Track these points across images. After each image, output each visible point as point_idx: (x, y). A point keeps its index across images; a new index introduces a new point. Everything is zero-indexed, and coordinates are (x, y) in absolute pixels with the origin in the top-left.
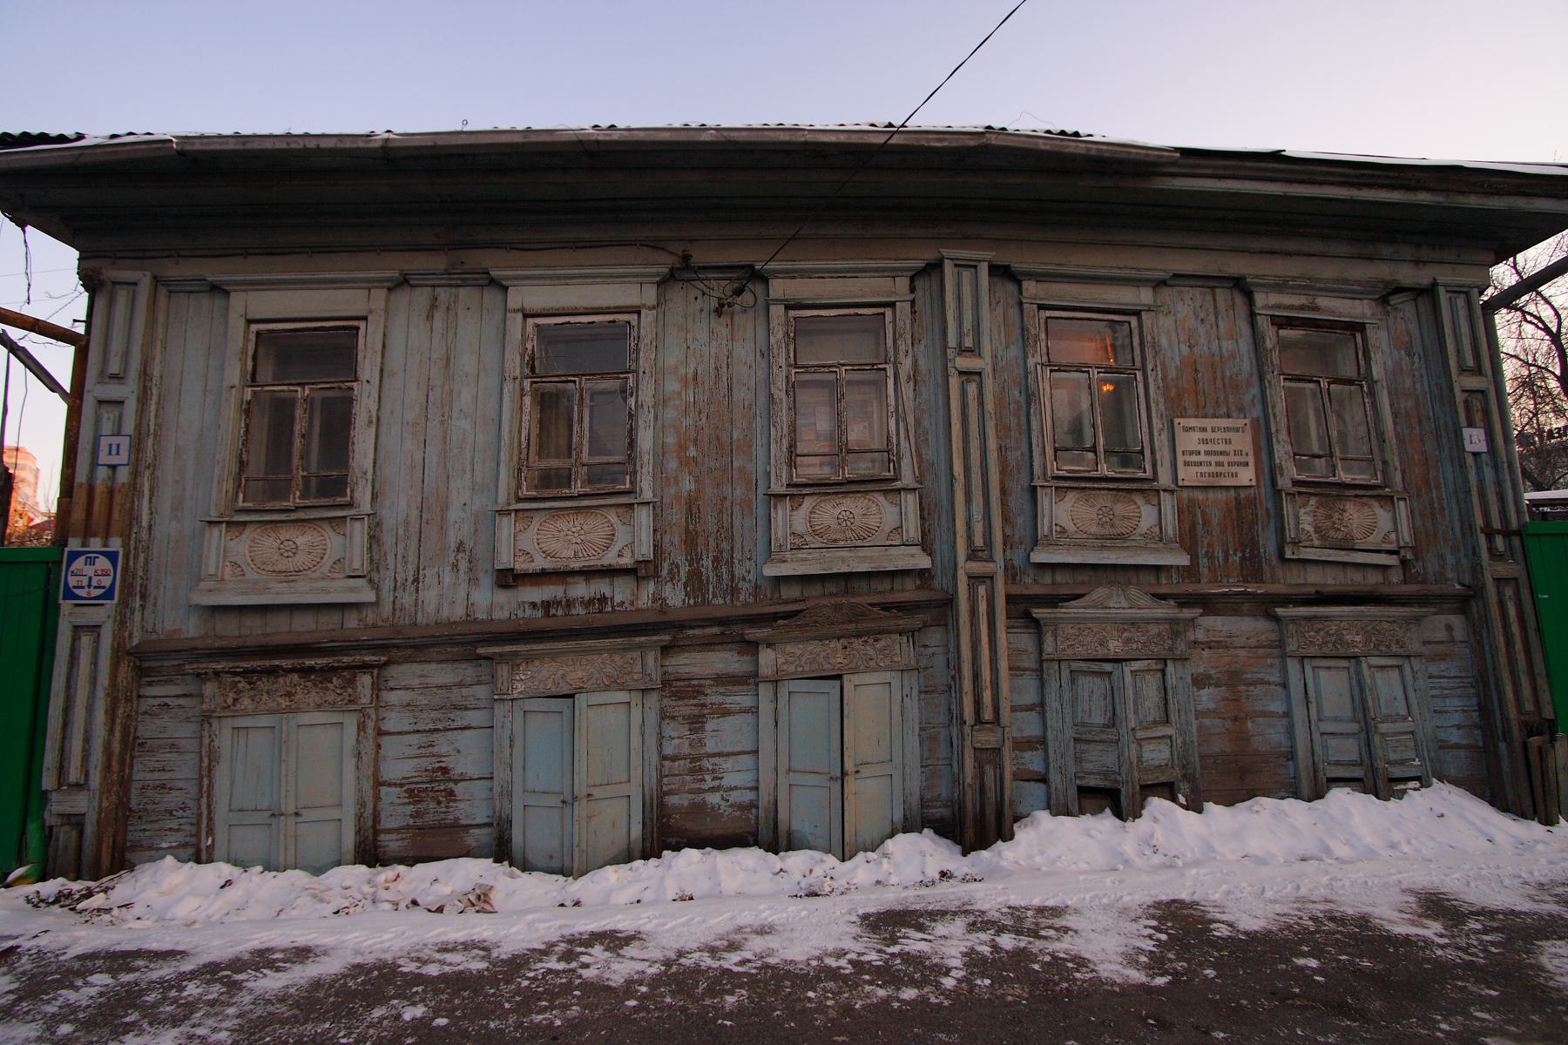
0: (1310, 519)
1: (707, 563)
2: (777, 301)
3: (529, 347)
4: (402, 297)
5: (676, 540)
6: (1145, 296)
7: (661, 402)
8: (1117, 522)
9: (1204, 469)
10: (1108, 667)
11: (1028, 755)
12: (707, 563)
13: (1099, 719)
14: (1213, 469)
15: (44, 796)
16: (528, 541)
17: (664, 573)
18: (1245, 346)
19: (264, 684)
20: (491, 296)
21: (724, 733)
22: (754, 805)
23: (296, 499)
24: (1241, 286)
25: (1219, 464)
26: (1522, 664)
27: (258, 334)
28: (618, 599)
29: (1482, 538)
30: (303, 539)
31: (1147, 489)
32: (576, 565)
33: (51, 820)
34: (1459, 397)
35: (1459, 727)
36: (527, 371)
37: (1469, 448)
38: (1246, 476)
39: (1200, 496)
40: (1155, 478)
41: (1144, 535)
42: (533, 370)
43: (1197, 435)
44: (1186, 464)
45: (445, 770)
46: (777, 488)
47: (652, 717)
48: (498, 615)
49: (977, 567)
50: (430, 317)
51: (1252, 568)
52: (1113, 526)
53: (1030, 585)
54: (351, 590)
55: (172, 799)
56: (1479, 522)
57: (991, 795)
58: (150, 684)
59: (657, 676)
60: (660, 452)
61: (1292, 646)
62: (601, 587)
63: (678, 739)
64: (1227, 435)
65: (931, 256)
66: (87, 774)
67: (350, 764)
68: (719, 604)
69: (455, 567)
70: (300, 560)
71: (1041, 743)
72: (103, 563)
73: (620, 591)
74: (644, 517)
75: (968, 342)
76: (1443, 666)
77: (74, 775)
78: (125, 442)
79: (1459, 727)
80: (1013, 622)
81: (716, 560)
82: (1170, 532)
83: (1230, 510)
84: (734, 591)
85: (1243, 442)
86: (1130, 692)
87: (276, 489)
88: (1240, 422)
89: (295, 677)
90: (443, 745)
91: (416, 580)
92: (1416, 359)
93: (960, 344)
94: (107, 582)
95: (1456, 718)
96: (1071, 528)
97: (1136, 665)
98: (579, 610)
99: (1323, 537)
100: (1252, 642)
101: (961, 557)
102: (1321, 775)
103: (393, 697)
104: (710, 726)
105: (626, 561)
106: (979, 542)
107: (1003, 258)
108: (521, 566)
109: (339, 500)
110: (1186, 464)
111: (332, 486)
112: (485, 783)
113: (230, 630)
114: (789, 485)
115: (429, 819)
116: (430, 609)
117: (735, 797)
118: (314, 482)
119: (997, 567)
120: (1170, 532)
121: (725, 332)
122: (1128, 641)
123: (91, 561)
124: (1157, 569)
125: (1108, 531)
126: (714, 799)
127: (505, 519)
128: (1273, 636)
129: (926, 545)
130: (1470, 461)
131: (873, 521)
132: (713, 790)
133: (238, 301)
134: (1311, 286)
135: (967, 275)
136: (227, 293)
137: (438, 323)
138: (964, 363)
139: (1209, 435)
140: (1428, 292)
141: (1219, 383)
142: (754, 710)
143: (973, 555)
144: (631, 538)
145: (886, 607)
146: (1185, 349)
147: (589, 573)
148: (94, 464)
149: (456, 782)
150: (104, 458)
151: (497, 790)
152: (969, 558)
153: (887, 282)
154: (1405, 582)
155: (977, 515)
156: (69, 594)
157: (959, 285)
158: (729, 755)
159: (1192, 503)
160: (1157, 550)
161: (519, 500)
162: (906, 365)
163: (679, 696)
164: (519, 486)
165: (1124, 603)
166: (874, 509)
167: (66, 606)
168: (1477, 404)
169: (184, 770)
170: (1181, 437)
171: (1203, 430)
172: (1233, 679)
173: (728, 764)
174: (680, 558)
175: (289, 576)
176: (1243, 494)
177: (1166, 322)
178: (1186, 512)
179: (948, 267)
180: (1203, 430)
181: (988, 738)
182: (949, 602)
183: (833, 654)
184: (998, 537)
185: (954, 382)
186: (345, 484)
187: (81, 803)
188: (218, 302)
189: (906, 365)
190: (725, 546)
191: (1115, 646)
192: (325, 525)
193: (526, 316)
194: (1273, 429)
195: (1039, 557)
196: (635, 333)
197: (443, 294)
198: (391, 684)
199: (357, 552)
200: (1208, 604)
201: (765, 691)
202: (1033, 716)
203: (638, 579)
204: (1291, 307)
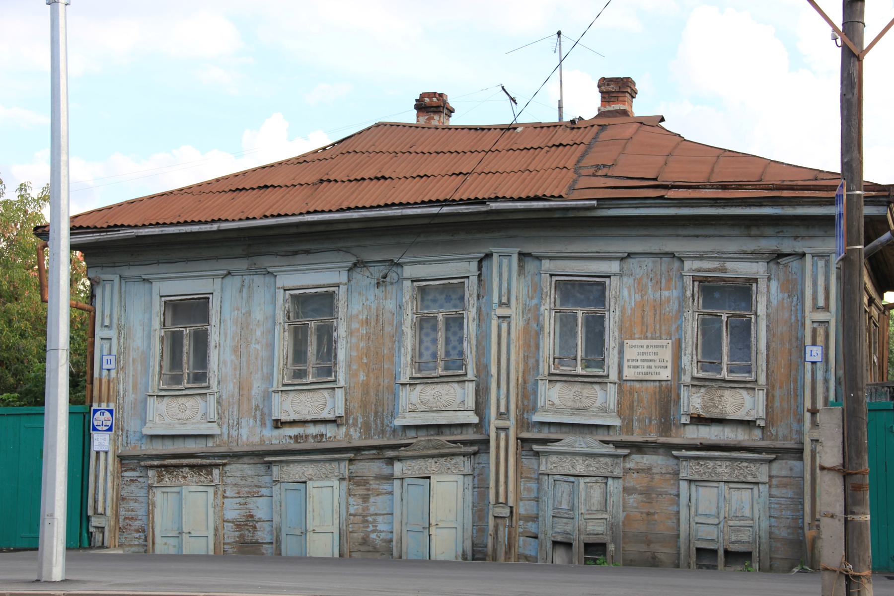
0: (699, 401)
2: (407, 279)
3: (287, 306)
4: (229, 280)
5: (356, 405)
6: (614, 267)
7: (350, 333)
8: (583, 399)
9: (639, 370)
10: (572, 479)
11: (530, 524)
13: (565, 506)
14: (645, 370)
15: (88, 518)
16: (287, 406)
17: (351, 422)
20: (268, 279)
21: (377, 504)
23: (185, 384)
27: (165, 302)
28: (328, 435)
29: (808, 416)
30: (189, 402)
31: (601, 381)
32: (309, 418)
36: (286, 319)
38: (666, 374)
39: (637, 385)
40: (607, 376)
41: (599, 408)
42: (289, 318)
44: (629, 367)
45: (252, 516)
48: (274, 442)
49: (501, 423)
50: (241, 291)
51: (666, 423)
52: (581, 402)
54: (209, 428)
56: (808, 404)
58: (126, 471)
59: (346, 475)
61: (683, 474)
63: (356, 506)
64: (656, 350)
66: (105, 509)
69: (255, 417)
71: (535, 518)
72: (107, 414)
73: (329, 431)
74: (340, 394)
75: (504, 300)
76: (784, 491)
77: (100, 510)
78: (113, 358)
81: (376, 413)
82: (612, 407)
83: (655, 393)
84: (383, 432)
85: (667, 355)
86: (583, 494)
87: (177, 379)
88: (664, 342)
89: (187, 469)
91: (238, 424)
92: (795, 299)
93: (500, 301)
94: (109, 423)
96: (557, 402)
97: (588, 480)
102: (692, 545)
103: (229, 480)
104: (372, 499)
105: (331, 417)
106: (503, 409)
107: (525, 251)
108: (284, 418)
109: (204, 385)
110: (629, 367)
111: (200, 377)
113: (160, 448)
114: (411, 378)
116: (245, 438)
117: (383, 535)
118: (191, 375)
119: (511, 423)
120: (612, 407)
121: (382, 295)
122: (588, 466)
124: (608, 427)
125: (578, 405)
126: (373, 536)
127: (276, 395)
130: (808, 366)
132: (374, 531)
133: (156, 286)
134: (720, 256)
135: (505, 261)
136: (151, 283)
137: (245, 291)
139: (645, 350)
141: (658, 317)
142: (391, 493)
146: (638, 297)
147: (315, 422)
148: (101, 368)
149: (257, 522)
150: (105, 366)
151: (274, 526)
153: (465, 265)
154: (763, 439)
156: (95, 429)
157: (500, 267)
158: (380, 515)
159: (632, 391)
160: (603, 417)
161: (284, 385)
163: (358, 484)
164: (283, 378)
165: (584, 445)
166: (452, 391)
168: (821, 331)
169: (141, 511)
171: (642, 347)
172: (648, 493)
173: (380, 519)
176: (664, 384)
182: (487, 442)
183: (431, 466)
186: (206, 377)
188: (147, 286)
190: (380, 409)
191: (580, 469)
192: (198, 398)
193: (285, 290)
194: (683, 346)
198: (228, 474)
199: (212, 410)
200: (639, 448)
201: (397, 483)
202: (533, 503)
203: (338, 426)
204: (709, 271)
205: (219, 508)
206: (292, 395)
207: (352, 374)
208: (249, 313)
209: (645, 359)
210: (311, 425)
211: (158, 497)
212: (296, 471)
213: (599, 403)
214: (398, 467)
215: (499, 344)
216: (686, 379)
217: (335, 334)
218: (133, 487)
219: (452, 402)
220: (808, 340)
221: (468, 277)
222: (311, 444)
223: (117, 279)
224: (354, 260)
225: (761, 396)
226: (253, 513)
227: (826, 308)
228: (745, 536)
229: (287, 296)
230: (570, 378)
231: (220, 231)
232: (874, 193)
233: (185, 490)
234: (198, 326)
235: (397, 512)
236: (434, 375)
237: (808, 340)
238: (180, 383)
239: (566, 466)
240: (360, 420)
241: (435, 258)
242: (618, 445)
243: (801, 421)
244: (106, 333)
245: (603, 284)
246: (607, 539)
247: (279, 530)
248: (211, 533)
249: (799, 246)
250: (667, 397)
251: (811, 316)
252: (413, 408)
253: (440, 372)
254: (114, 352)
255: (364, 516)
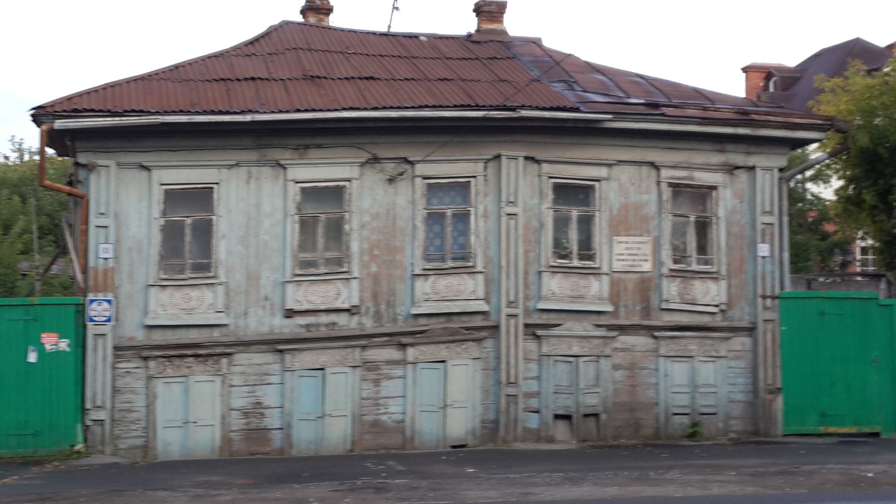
1: (383, 307)
2: (419, 176)
6: (603, 172)
7: (363, 226)
10: (571, 359)
12: (383, 307)
18: (654, 197)
19: (177, 362)
21: (390, 388)
22: (403, 421)
24: (652, 164)
25: (634, 260)
26: (770, 362)
30: (194, 293)
31: (596, 273)
32: (322, 307)
33: (89, 423)
34: (759, 227)
35: (742, 392)
37: (761, 254)
38: (647, 267)
39: (623, 276)
43: (625, 245)
44: (618, 260)
45: (259, 403)
46: (418, 272)
47: (357, 379)
50: (248, 182)
51: (646, 312)
53: (536, 319)
54: (219, 318)
55: (134, 415)
57: (512, 416)
58: (119, 362)
60: (362, 252)
61: (663, 351)
62: (333, 318)
63: (368, 390)
65: (495, 152)
67: (218, 399)
68: (388, 328)
70: (193, 304)
71: (537, 394)
74: (355, 284)
79: (742, 392)
80: (527, 337)
84: (395, 320)
85: (647, 249)
90: (260, 391)
93: (508, 199)
95: (741, 388)
96: (557, 291)
98: (323, 329)
99: (681, 299)
100: (644, 349)
101: (504, 302)
105: (346, 306)
108: (297, 307)
110: (618, 260)
111: (204, 266)
112: (280, 410)
113: (159, 338)
115: (253, 426)
117: (395, 417)
119: (519, 311)
123: (100, 304)
125: (576, 294)
126: (384, 418)
128: (654, 346)
129: (487, 300)
131: (462, 288)
132: (385, 413)
135: (513, 163)
136: (285, 168)
138: (510, 210)
140: (752, 169)
142: (404, 377)
143: (510, 304)
144: (347, 294)
145: (467, 329)
146: (623, 200)
152: (508, 307)
155: (512, 286)
159: (620, 280)
162: (481, 208)
163: (369, 370)
167: (89, 324)
169: (140, 402)
170: (616, 245)
171: (627, 243)
173: (390, 402)
174: (370, 304)
175: (190, 311)
177: (614, 185)
178: (614, 284)
179: (504, 159)
180: (627, 243)
181: (511, 391)
183: (442, 351)
184: (521, 296)
185: (504, 219)
187: (102, 415)
188: (144, 174)
189: (481, 208)
191: (576, 350)
195: (541, 306)
196: (348, 192)
197: (254, 170)
198: (235, 363)
200: (623, 329)
202: (535, 382)
204: (679, 179)
205: (226, 397)
206: (305, 284)
207: (364, 266)
208: (258, 206)
209: (627, 253)
210: (323, 314)
211: (160, 386)
212: (309, 358)
213: (595, 292)
214: (411, 353)
215: (508, 239)
216: (665, 271)
217: (347, 227)
218: (128, 379)
219: (465, 292)
220: (759, 239)
221: (474, 177)
222: (323, 332)
223: (113, 167)
224: (369, 156)
225: (723, 284)
226: (262, 400)
227: (771, 213)
228: (710, 401)
229: (298, 189)
230: (568, 271)
231: (484, 119)
232: (820, 122)
233: (193, 379)
234: (201, 216)
235: (410, 395)
236: (446, 266)
237: (759, 239)
238: (182, 272)
239: (563, 348)
240: (372, 309)
241: (441, 158)
242: (611, 328)
243: (754, 304)
244: (102, 221)
245: (592, 188)
246: (599, 410)
247: (290, 414)
248: (217, 422)
249: (751, 161)
250: (646, 287)
251: (762, 219)
252: (426, 297)
253: (450, 264)
254: (112, 239)
255: (377, 399)
